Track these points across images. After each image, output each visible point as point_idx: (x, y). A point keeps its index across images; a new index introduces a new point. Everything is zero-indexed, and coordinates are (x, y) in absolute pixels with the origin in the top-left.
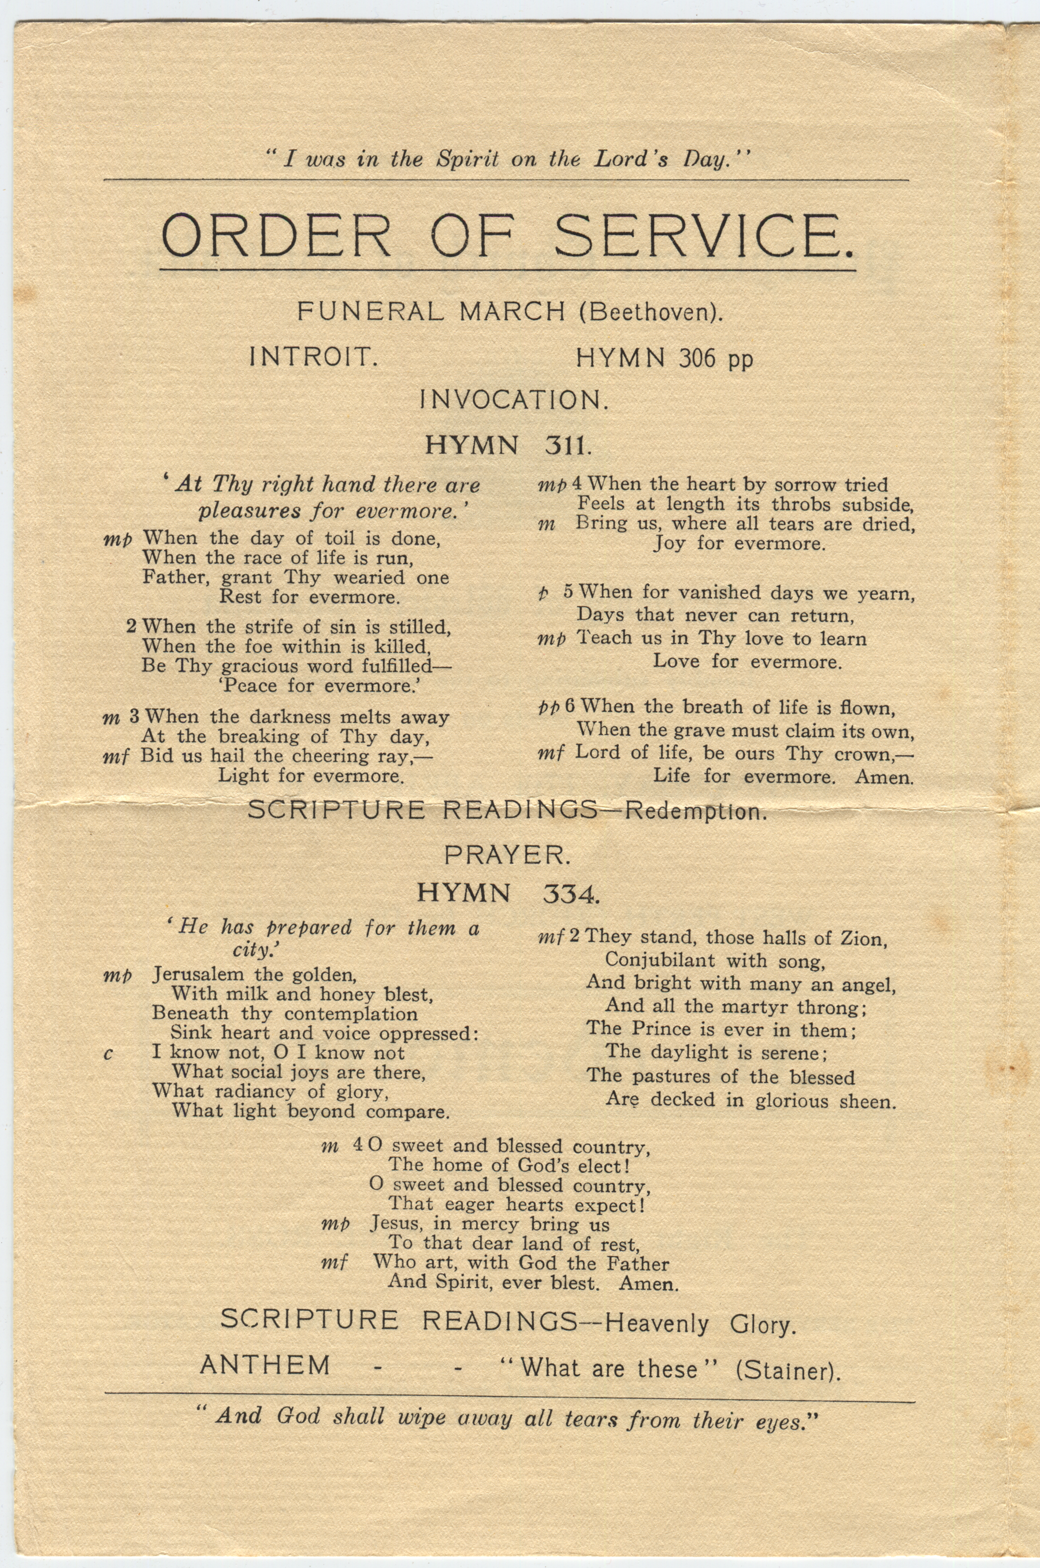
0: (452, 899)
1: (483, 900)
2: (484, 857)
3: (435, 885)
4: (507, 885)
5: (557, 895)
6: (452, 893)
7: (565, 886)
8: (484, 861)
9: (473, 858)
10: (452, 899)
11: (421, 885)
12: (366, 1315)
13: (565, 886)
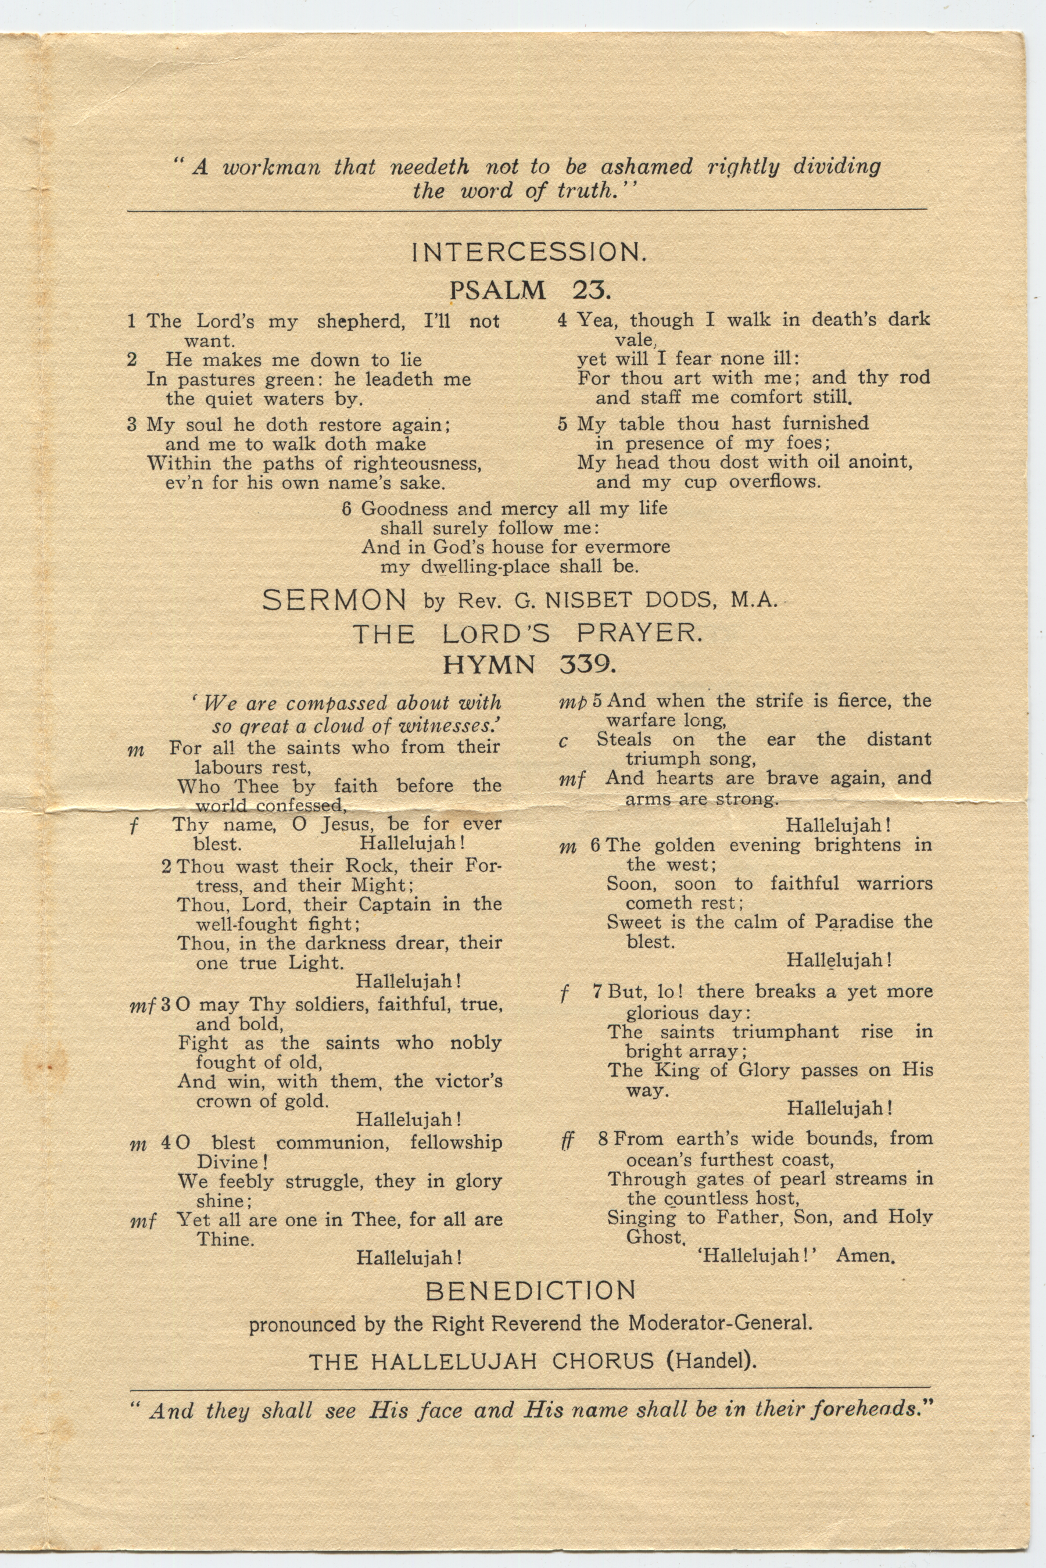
0: (477, 671)
1: (509, 671)
2: (617, 634)
3: (461, 658)
4: (532, 657)
5: (573, 665)
6: (477, 665)
7: (581, 656)
8: (617, 637)
9: (606, 635)
10: (477, 671)
11: (447, 658)
12: (494, 247)
13: (581, 656)
